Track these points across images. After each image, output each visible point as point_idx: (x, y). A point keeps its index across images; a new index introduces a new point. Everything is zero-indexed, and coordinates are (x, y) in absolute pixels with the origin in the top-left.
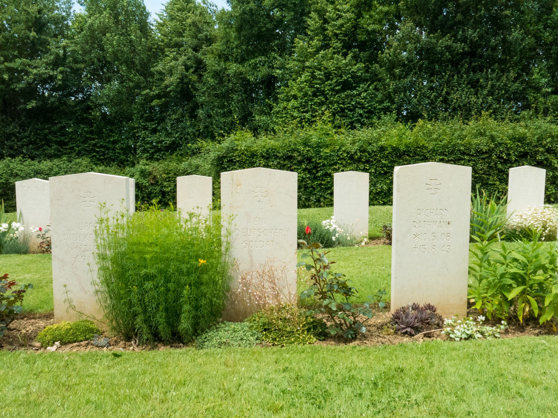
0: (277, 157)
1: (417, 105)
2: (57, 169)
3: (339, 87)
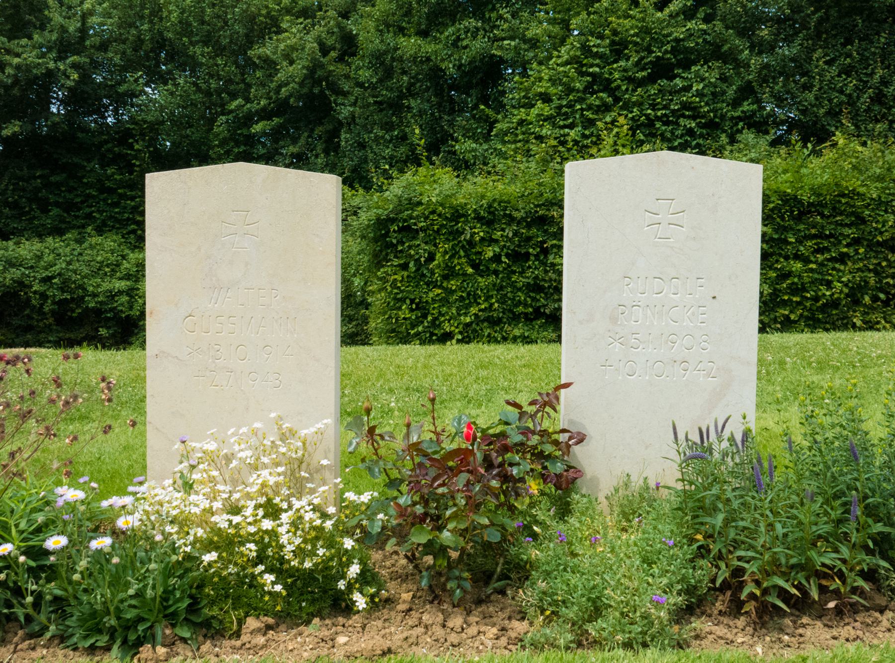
0: (511, 219)
1: (813, 106)
2: (51, 257)
3: (644, 73)
